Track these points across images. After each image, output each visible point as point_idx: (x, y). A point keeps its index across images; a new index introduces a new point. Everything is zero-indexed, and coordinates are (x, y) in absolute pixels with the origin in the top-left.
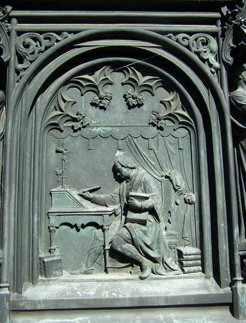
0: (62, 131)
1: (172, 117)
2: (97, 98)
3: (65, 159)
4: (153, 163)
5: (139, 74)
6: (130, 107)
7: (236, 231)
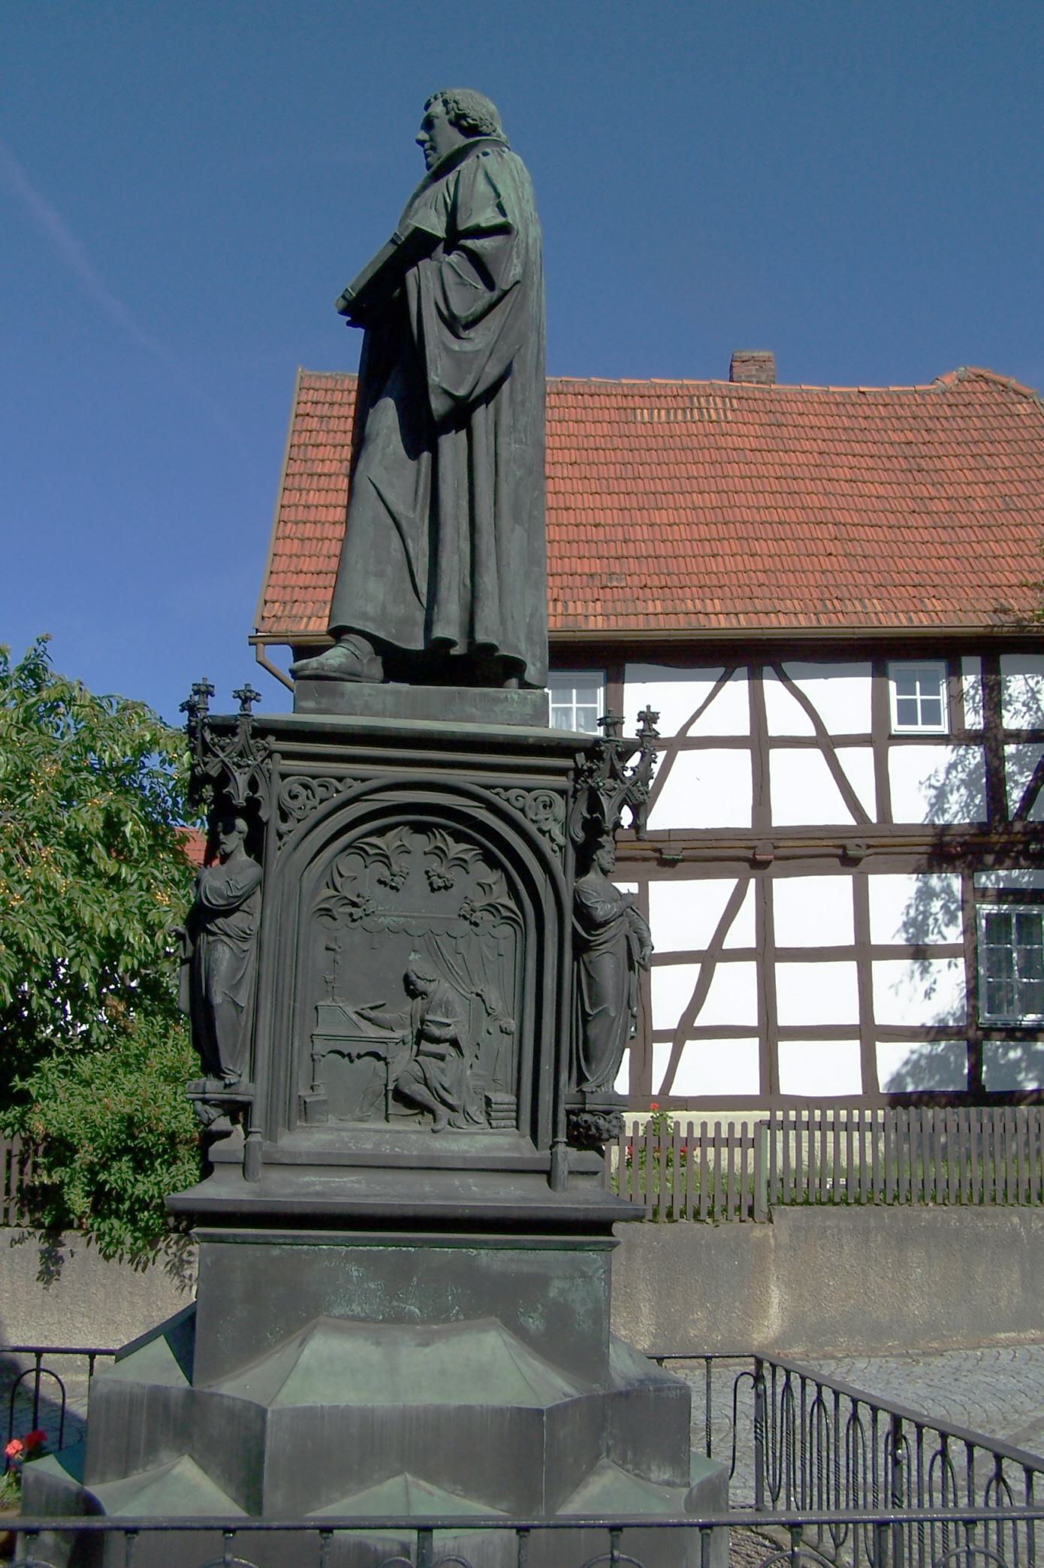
0: (335, 919)
1: (492, 908)
2: (388, 873)
3: (268, 813)
5: (449, 839)
6: (433, 890)
7: (564, 1076)
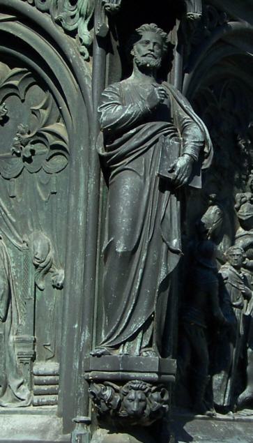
4: (14, 220)
